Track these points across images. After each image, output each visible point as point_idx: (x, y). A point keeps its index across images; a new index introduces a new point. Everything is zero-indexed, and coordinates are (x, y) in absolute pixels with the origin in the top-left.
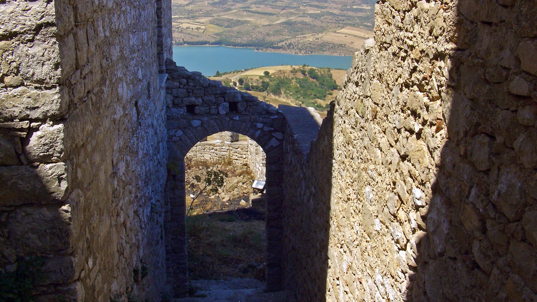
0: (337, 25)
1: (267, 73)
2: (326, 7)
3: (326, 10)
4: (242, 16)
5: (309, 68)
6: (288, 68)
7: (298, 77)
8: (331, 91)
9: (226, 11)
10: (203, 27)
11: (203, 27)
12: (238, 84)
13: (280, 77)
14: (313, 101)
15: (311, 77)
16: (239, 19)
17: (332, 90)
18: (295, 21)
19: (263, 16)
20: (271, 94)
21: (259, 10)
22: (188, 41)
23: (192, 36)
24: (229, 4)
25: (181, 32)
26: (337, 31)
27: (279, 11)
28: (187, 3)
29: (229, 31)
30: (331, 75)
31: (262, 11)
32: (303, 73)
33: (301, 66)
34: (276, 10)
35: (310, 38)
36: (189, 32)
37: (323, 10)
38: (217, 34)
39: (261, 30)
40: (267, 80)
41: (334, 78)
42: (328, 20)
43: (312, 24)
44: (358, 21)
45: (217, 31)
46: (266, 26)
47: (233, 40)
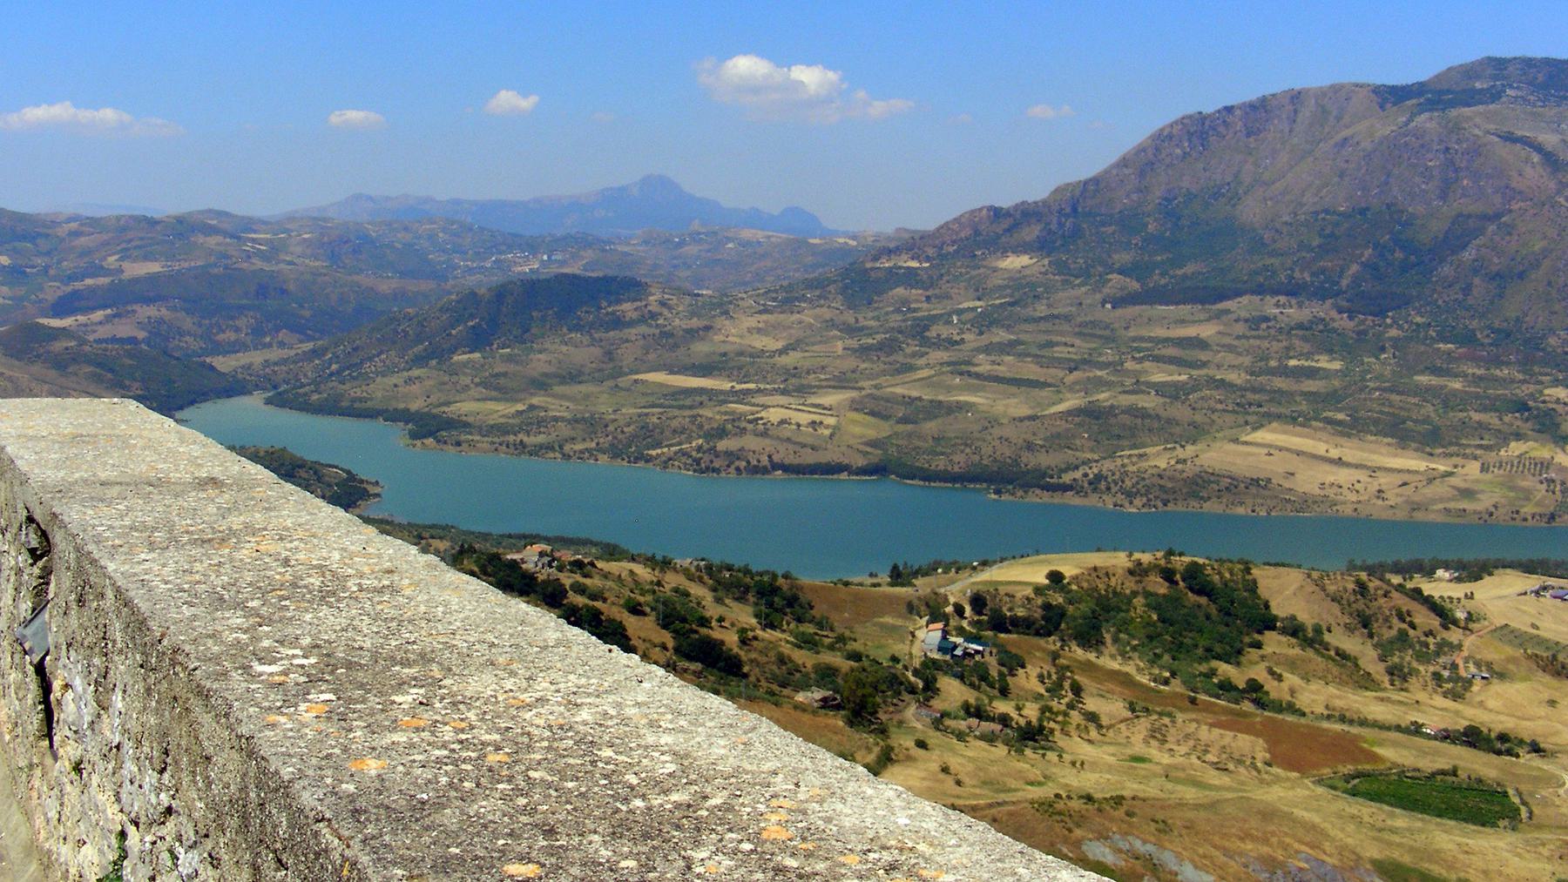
0: (1241, 420)
1: (1056, 577)
2: (1204, 364)
3: (1204, 372)
4: (949, 389)
5: (1187, 559)
6: (1119, 560)
7: (1150, 589)
8: (1257, 636)
9: (898, 372)
10: (831, 421)
11: (831, 421)
12: (968, 609)
13: (1096, 589)
14: (1203, 668)
15: (1191, 589)
16: (941, 398)
17: (1260, 632)
18: (1112, 407)
19: (1014, 389)
20: (1074, 647)
21: (1001, 370)
22: (787, 461)
23: (798, 448)
24: (909, 350)
25: (764, 434)
26: (1244, 438)
27: (1061, 373)
28: (780, 345)
29: (910, 435)
30: (1255, 582)
31: (1008, 375)
32: (1168, 575)
33: (1160, 554)
34: (1052, 371)
35: (1159, 459)
36: (789, 434)
37: (1195, 373)
38: (873, 444)
39: (1008, 432)
40: (1058, 599)
41: (1263, 591)
42: (1212, 403)
43: (1163, 414)
44: (1304, 407)
45: (872, 434)
46: (1021, 420)
47: (921, 462)
